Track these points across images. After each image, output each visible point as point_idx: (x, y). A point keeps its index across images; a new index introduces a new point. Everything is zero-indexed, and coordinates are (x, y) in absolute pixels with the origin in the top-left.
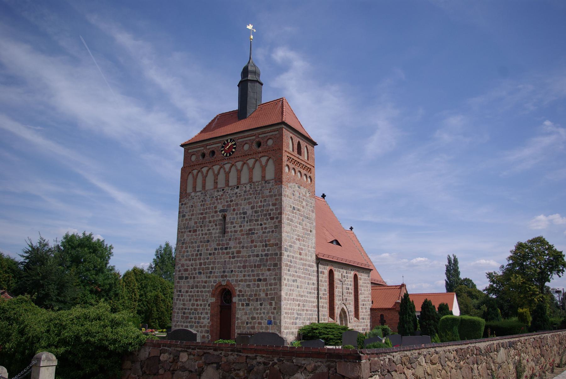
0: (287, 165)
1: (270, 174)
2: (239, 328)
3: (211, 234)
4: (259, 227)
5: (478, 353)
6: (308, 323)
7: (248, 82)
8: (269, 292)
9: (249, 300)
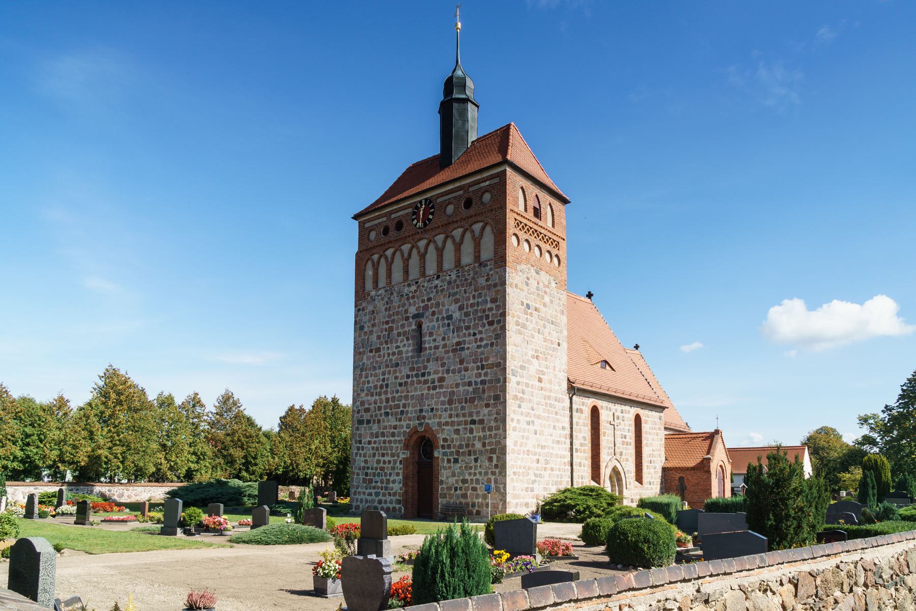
0: (515, 235)
1: (487, 252)
2: (444, 496)
3: (400, 353)
4: (472, 338)
5: (871, 578)
6: (554, 490)
7: (452, 104)
8: (487, 441)
9: (458, 453)
